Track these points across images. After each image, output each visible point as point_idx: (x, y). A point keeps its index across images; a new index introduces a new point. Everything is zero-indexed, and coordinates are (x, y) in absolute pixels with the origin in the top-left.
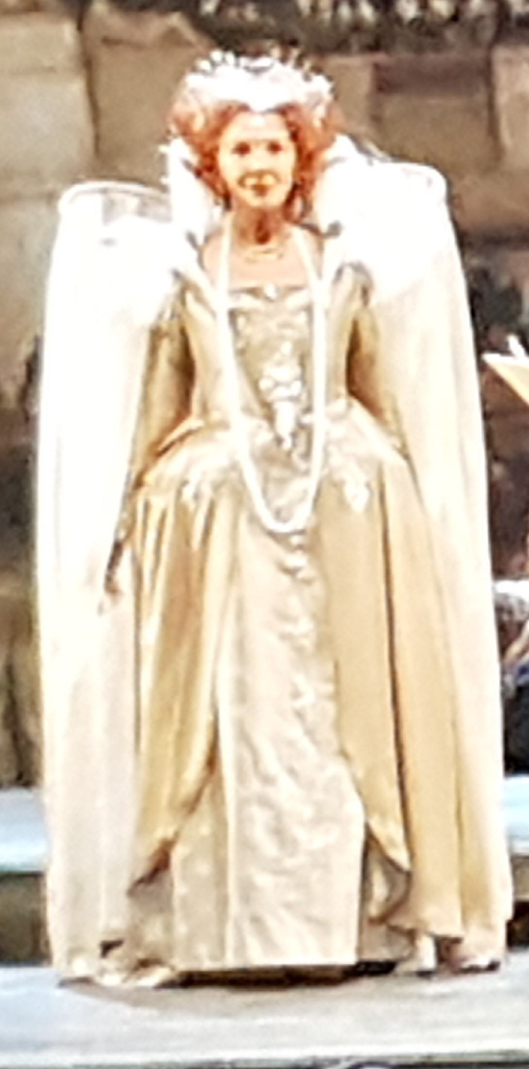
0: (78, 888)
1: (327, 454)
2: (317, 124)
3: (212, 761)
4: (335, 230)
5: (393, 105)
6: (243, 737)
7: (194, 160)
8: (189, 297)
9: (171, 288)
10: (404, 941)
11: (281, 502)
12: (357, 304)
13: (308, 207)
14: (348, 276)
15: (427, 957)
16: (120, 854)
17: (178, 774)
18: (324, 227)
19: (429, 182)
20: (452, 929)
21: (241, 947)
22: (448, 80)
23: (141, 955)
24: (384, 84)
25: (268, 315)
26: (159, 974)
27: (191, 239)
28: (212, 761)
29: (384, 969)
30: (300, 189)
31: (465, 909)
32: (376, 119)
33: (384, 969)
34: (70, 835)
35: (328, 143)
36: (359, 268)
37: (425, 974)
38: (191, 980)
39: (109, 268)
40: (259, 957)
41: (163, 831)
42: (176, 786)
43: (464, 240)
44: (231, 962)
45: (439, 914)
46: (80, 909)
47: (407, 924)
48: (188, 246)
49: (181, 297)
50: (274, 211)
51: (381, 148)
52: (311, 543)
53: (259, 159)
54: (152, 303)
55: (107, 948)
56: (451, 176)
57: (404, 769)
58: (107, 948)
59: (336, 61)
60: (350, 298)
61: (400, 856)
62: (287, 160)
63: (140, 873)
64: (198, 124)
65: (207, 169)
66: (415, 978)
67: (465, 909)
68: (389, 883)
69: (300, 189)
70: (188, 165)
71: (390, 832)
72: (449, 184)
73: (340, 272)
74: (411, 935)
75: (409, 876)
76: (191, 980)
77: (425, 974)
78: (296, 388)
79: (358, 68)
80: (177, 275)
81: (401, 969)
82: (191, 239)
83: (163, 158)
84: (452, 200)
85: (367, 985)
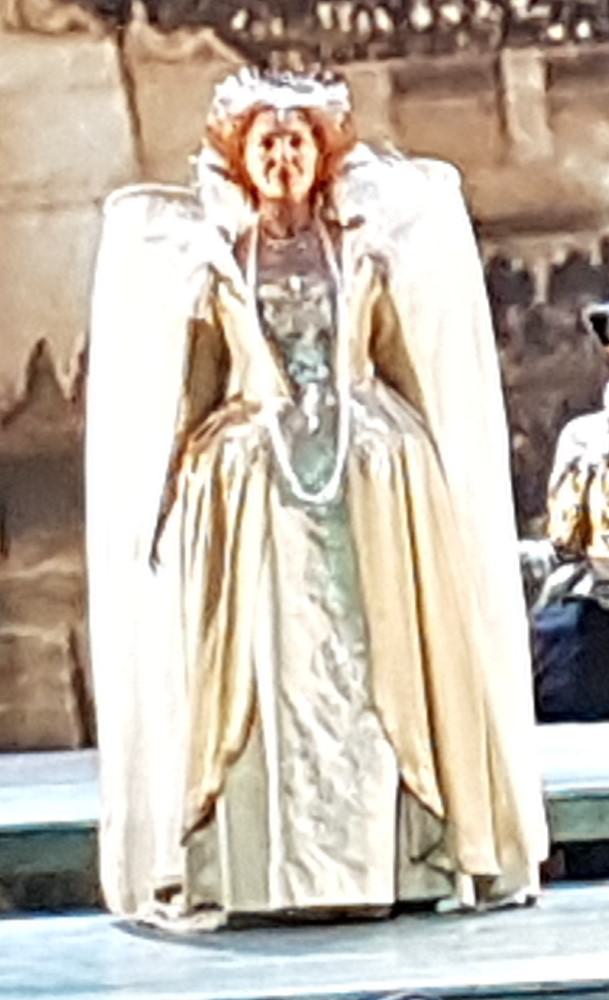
0: (131, 833)
1: (352, 435)
2: (337, 127)
3: (252, 716)
4: (356, 223)
5: (412, 105)
6: (282, 695)
7: (222, 163)
8: (223, 288)
9: (204, 279)
10: (441, 879)
11: (310, 478)
12: (378, 290)
13: (328, 201)
14: (368, 264)
15: (468, 896)
16: (172, 811)
17: (221, 737)
18: (344, 222)
19: (446, 177)
20: (489, 867)
21: (291, 895)
22: (461, 81)
23: (197, 900)
24: (401, 87)
25: (296, 74)
26: (212, 920)
27: (225, 234)
28: (252, 716)
29: (424, 908)
30: (322, 185)
31: (499, 835)
32: (396, 121)
33: (424, 908)
34: (127, 790)
35: (348, 147)
36: (378, 259)
37: (464, 911)
38: (243, 924)
39: (144, 278)
40: (304, 900)
41: (210, 784)
42: (221, 737)
43: (481, 228)
44: (276, 902)
45: (478, 853)
46: (138, 858)
47: (446, 863)
48: (222, 240)
49: (215, 289)
50: (303, 745)
51: (399, 148)
52: (341, 511)
53: (282, 149)
54: (183, 302)
55: (166, 895)
56: (463, 168)
57: (444, 775)
58: (166, 895)
59: (349, 70)
60: (373, 284)
61: (439, 810)
62: (309, 152)
63: (190, 823)
64: (228, 130)
65: (237, 174)
66: (457, 916)
67: (499, 835)
68: (427, 836)
69: (322, 185)
70: (215, 169)
71: (424, 781)
72: (463, 175)
73: (360, 263)
74: (451, 877)
75: (444, 822)
76: (243, 924)
77: (464, 911)
78: (323, 372)
79: (375, 75)
80: (211, 268)
81: (443, 906)
82: (225, 234)
83: (194, 167)
84: (468, 193)
85: (407, 922)
